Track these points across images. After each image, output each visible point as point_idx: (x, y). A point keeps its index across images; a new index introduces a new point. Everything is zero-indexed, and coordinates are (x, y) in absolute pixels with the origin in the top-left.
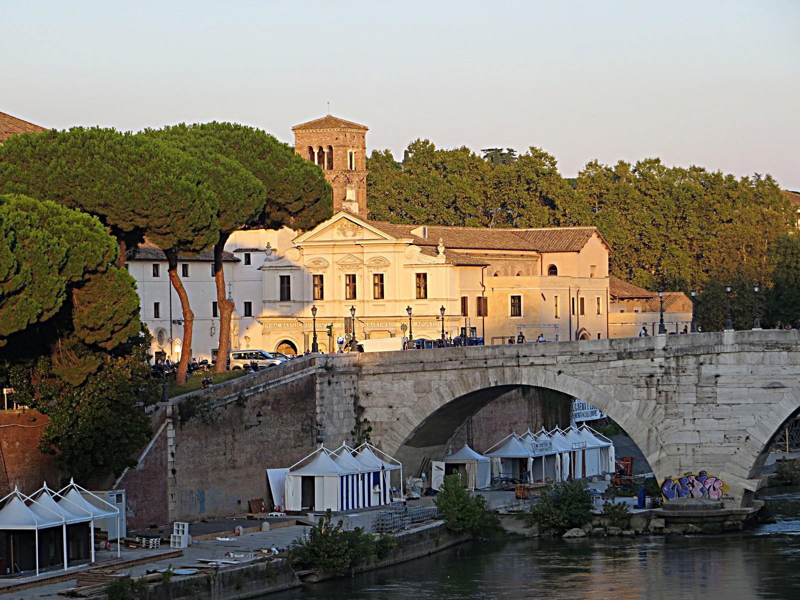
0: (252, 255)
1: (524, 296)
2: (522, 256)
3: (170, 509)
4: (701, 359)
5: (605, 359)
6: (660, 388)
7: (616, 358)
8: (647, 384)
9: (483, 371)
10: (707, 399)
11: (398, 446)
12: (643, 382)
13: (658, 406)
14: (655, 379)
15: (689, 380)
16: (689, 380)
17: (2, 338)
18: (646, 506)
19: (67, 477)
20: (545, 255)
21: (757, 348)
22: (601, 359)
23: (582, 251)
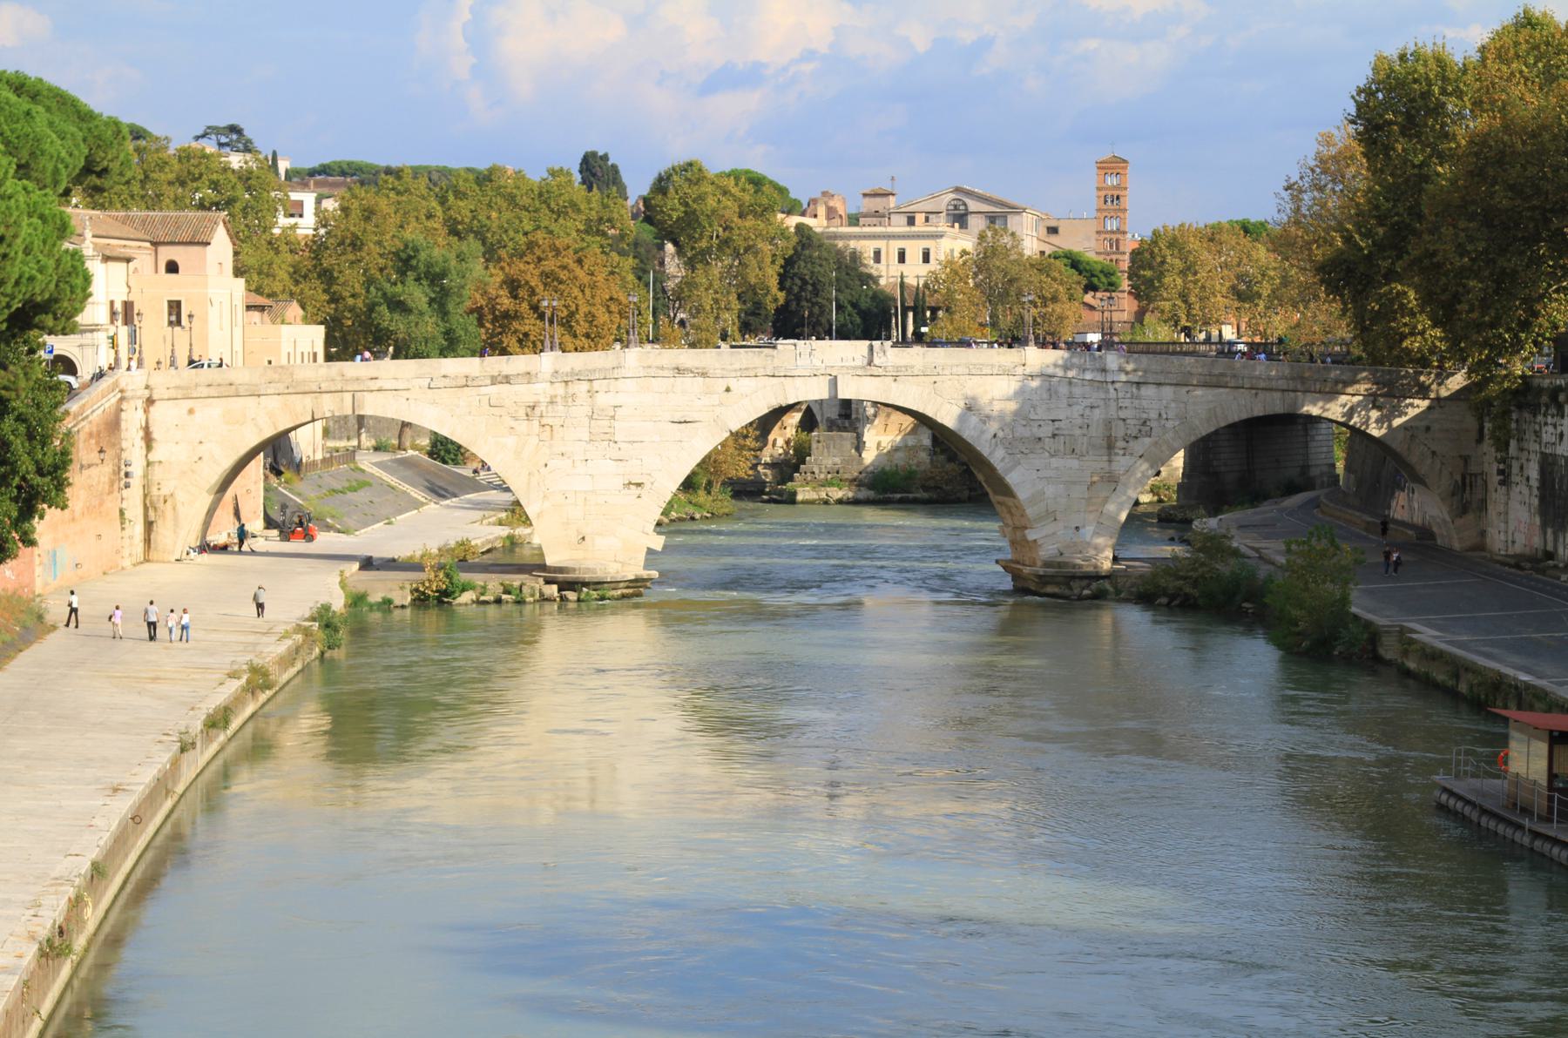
0: (931, 216)
1: (186, 300)
2: (125, 246)
3: (37, 574)
4: (596, 385)
5: (475, 383)
6: (544, 421)
7: (489, 382)
8: (527, 415)
9: (316, 398)
10: (602, 435)
11: (1355, 423)
12: (521, 413)
13: (541, 443)
14: (537, 412)
15: (580, 411)
16: (580, 411)
17: (2, 323)
18: (564, 593)
19: (1176, 445)
20: (161, 249)
21: (666, 373)
22: (469, 383)
23: (212, 242)
